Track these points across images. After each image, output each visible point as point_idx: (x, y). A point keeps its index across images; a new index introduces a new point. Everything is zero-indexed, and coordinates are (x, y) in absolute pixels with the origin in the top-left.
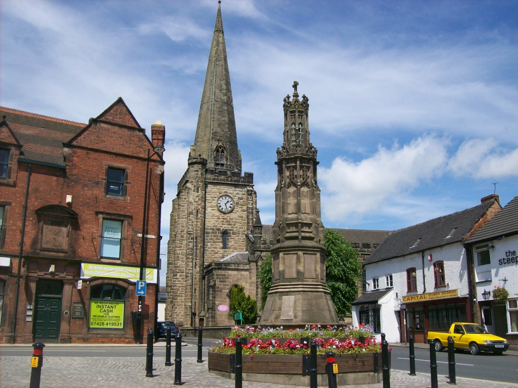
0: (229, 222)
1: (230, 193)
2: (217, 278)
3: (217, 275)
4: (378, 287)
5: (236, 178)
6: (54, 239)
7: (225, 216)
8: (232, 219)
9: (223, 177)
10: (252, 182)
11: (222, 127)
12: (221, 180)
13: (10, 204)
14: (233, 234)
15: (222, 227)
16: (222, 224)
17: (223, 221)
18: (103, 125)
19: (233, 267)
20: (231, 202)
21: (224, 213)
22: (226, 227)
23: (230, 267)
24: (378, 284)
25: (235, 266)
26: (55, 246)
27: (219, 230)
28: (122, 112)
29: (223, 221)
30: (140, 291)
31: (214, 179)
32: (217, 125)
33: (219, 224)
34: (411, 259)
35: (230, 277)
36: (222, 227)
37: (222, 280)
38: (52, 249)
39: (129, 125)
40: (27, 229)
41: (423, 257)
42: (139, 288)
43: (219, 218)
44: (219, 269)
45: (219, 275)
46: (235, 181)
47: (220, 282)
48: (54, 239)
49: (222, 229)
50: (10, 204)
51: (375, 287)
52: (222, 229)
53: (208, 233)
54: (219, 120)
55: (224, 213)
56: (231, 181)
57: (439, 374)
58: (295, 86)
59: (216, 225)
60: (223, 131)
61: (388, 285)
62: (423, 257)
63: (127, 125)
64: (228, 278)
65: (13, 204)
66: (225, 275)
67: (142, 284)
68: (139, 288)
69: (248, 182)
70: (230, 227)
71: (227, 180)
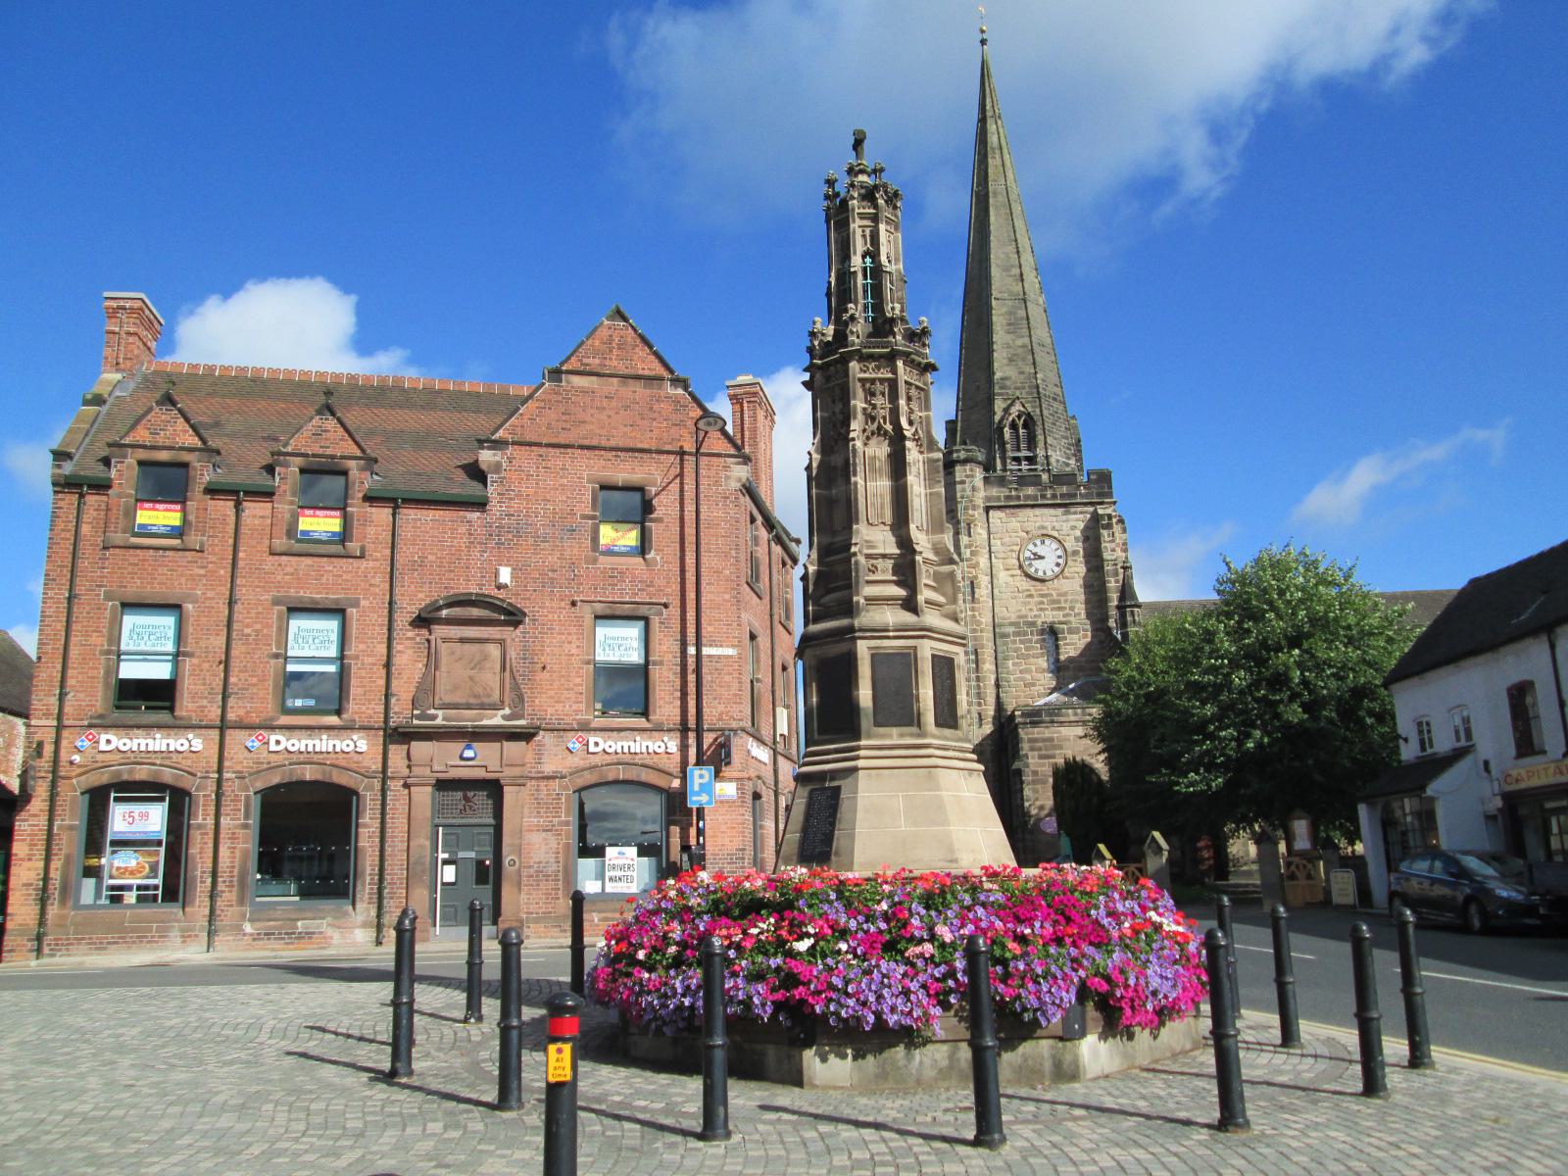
0: (1059, 602)
1: (1054, 528)
2: (1032, 749)
3: (1030, 741)
4: (1431, 747)
5: (1065, 489)
6: (471, 678)
7: (1044, 588)
8: (1065, 594)
9: (1030, 491)
10: (1110, 495)
11: (1020, 363)
12: (1027, 497)
13: (356, 603)
14: (1071, 631)
15: (1039, 616)
16: (1041, 609)
17: (1043, 603)
18: (576, 380)
19: (1072, 718)
20: (1031, 547)
21: (1042, 581)
22: (1050, 616)
23: (1062, 719)
24: (1430, 740)
25: (1076, 714)
26: (475, 696)
27: (1033, 624)
28: (625, 343)
29: (1043, 603)
30: (698, 794)
31: (1008, 498)
32: (1005, 361)
33: (1031, 610)
34: (301, 602)
35: (1065, 744)
36: (1039, 616)
37: (1043, 752)
38: (468, 704)
39: (646, 373)
40: (399, 661)
41: (1553, 647)
42: (696, 788)
43: (1031, 596)
44: (1034, 724)
45: (1036, 740)
46: (1063, 496)
47: (1041, 757)
48: (471, 678)
49: (1039, 623)
50: (356, 603)
51: (1423, 749)
52: (1039, 623)
53: (1005, 635)
54: (1008, 346)
55: (1042, 581)
56: (1054, 496)
57: (1386, 1035)
58: (858, 143)
59: (1024, 612)
60: (1023, 373)
61: (1458, 739)
62: (1553, 647)
63: (640, 372)
64: (1060, 747)
65: (363, 603)
66: (1051, 740)
67: (701, 776)
68: (696, 788)
69: (1099, 495)
70: (1058, 616)
71: (1043, 497)
